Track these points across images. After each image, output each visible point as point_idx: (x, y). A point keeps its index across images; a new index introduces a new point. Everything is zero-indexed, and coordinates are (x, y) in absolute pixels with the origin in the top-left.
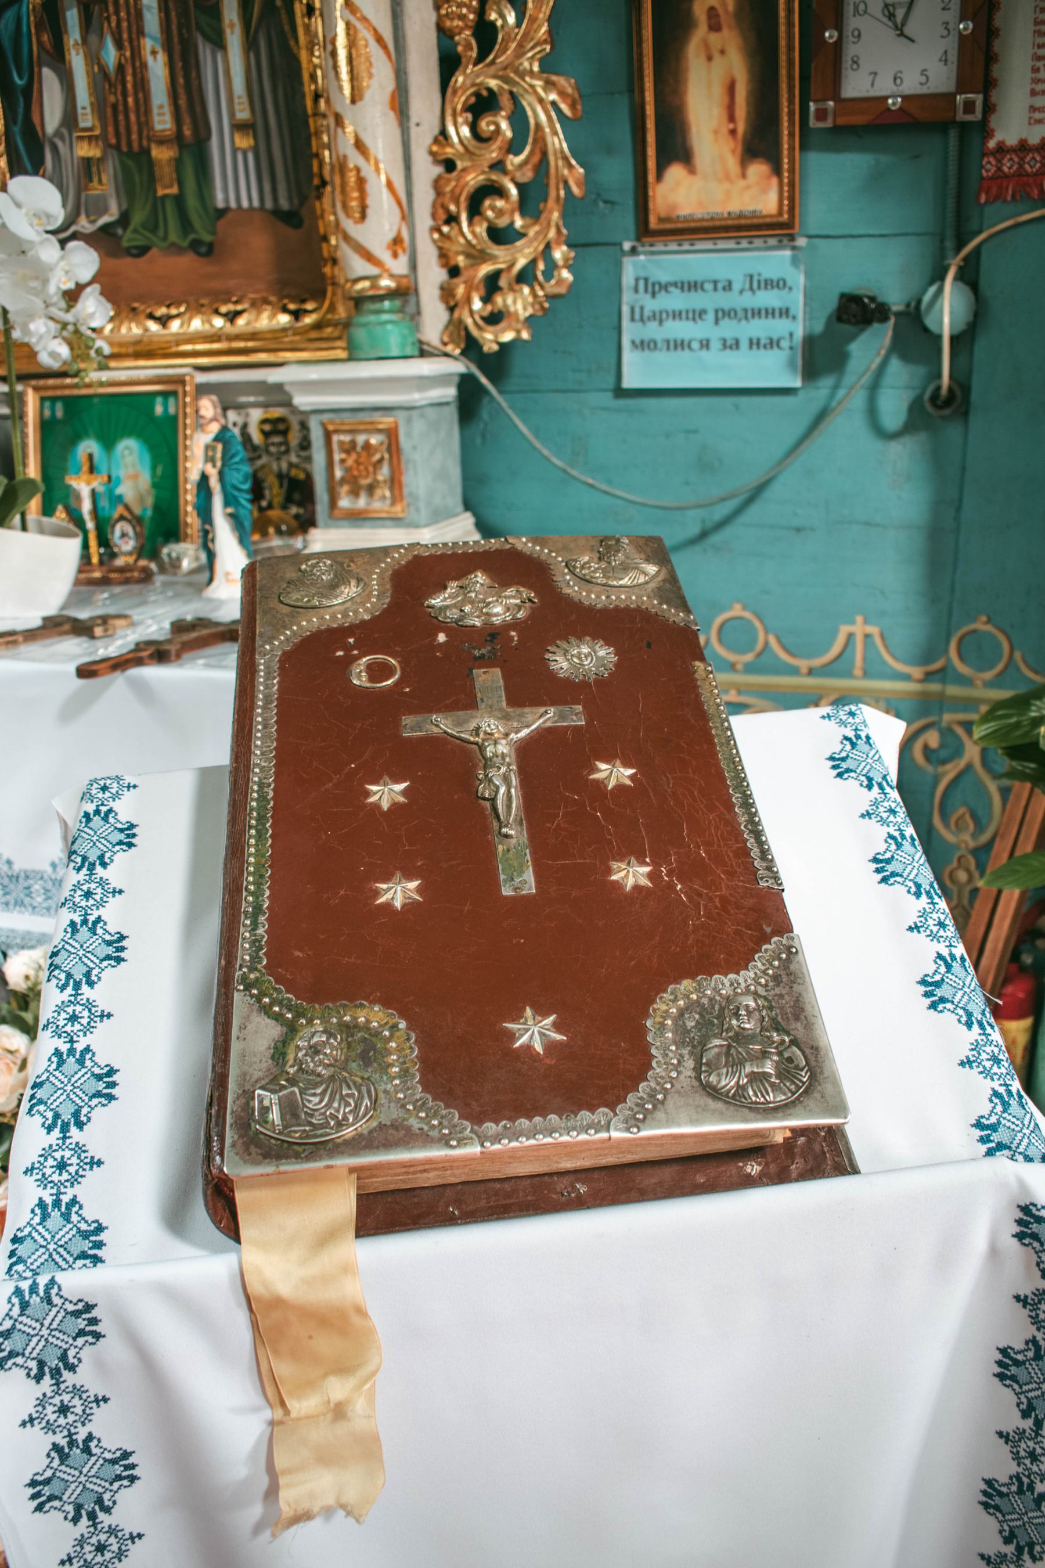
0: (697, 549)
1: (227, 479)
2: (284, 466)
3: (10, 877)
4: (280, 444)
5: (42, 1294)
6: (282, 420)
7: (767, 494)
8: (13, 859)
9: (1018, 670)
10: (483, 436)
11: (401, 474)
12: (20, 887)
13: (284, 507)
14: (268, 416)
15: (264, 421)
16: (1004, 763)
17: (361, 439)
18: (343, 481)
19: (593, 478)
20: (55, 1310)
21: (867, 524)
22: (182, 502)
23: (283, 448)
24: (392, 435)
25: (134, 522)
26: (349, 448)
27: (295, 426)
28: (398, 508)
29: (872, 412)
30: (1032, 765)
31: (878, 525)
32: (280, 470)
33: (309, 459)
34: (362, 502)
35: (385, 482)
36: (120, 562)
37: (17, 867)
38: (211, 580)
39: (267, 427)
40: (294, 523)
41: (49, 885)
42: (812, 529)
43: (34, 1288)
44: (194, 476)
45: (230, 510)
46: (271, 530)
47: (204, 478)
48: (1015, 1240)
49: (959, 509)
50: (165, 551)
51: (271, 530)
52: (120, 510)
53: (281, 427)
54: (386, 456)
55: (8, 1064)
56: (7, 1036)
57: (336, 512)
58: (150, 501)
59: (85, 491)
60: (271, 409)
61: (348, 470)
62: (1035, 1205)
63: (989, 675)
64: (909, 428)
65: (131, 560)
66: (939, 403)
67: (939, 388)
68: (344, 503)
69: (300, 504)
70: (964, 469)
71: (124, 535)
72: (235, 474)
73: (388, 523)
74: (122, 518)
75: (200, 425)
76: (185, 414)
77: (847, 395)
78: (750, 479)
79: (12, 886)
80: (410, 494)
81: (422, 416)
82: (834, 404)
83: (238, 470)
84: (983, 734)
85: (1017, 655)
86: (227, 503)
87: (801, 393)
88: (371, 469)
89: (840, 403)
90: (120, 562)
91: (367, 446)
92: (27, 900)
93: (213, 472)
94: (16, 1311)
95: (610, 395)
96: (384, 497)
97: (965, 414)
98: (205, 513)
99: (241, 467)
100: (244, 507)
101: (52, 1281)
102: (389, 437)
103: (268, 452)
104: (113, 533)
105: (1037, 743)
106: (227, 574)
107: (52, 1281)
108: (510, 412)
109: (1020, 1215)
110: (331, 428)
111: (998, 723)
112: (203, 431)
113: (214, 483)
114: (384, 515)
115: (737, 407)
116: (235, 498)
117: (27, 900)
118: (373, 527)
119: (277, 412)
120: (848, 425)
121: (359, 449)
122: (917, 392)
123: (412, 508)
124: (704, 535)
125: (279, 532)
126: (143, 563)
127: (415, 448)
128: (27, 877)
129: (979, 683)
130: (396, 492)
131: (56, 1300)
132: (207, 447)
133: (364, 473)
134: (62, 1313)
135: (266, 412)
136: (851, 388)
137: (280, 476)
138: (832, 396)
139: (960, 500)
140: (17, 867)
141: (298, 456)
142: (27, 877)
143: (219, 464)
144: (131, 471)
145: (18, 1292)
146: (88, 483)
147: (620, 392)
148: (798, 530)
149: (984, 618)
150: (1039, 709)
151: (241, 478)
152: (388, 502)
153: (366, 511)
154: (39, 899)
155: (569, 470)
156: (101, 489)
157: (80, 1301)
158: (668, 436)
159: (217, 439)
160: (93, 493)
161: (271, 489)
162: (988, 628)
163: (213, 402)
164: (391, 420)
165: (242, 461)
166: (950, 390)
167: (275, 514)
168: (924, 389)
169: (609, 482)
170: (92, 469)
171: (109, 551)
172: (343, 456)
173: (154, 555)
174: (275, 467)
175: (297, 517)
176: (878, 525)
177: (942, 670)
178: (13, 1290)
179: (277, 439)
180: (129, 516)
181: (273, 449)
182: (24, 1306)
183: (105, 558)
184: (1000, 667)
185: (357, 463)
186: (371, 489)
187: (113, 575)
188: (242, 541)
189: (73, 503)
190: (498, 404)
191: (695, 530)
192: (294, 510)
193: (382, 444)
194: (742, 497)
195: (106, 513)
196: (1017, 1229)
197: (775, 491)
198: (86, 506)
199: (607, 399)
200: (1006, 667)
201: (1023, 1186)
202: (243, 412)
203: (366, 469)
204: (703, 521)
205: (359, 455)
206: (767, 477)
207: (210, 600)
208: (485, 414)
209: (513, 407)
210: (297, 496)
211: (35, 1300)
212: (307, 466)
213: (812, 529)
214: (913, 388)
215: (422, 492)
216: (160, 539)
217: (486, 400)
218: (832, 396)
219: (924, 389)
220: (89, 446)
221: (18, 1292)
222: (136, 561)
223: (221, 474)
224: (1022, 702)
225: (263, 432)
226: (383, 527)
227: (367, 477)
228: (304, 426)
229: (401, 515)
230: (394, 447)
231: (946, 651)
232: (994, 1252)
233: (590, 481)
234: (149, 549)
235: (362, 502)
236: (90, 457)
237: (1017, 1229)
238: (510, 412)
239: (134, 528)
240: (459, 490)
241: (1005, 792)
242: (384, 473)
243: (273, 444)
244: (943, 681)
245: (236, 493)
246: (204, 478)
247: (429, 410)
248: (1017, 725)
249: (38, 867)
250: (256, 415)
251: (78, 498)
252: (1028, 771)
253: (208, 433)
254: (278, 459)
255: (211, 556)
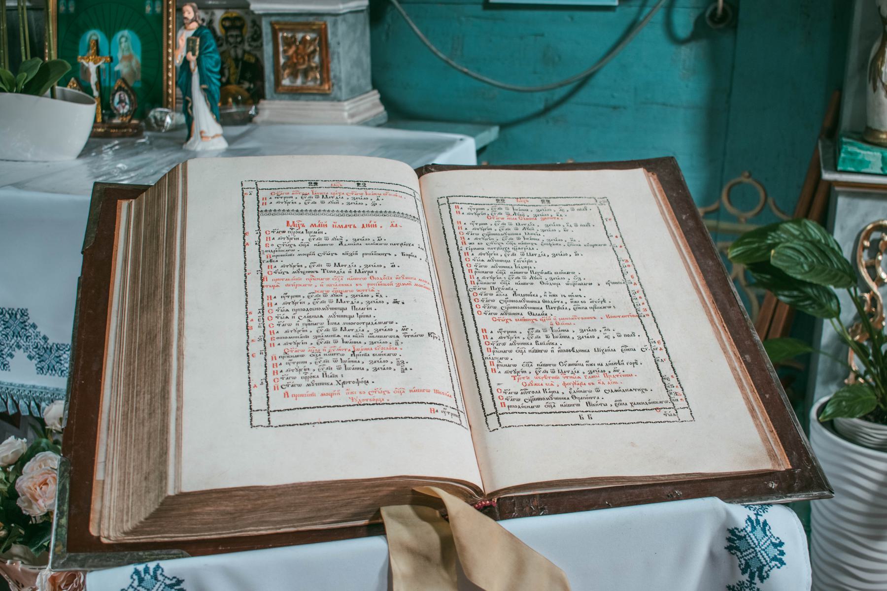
0: (542, 120)
2: (240, 52)
3: (45, 349)
4: (237, 36)
5: (152, 573)
6: (238, 18)
7: (593, 81)
8: (48, 336)
11: (328, 62)
12: (53, 356)
13: (239, 83)
14: (229, 15)
15: (224, 19)
17: (299, 36)
18: (285, 65)
20: (159, 583)
21: (664, 104)
23: (239, 39)
24: (322, 35)
26: (289, 43)
27: (249, 24)
30: (768, 277)
31: (671, 106)
32: (237, 56)
33: (260, 47)
35: (317, 68)
36: (117, 121)
39: (227, 24)
40: (246, 94)
42: (625, 108)
43: (146, 570)
44: (178, 61)
45: (204, 86)
47: (186, 62)
48: (725, 552)
52: (119, 82)
53: (238, 24)
54: (318, 49)
58: (139, 77)
59: (93, 68)
61: (289, 58)
62: (737, 529)
63: (750, 214)
65: (126, 120)
67: (716, 9)
68: (286, 82)
72: (209, 60)
73: (318, 97)
74: (120, 89)
75: (182, 23)
78: (580, 71)
79: (46, 356)
80: (335, 77)
81: (344, 20)
82: (641, 18)
83: (211, 58)
84: (734, 254)
85: (770, 201)
86: (202, 82)
87: (618, 10)
88: (306, 58)
89: (646, 17)
91: (304, 40)
93: (192, 58)
94: (136, 583)
95: (480, 7)
97: (735, 27)
99: (213, 55)
100: (214, 84)
101: (158, 567)
102: (320, 35)
103: (227, 42)
104: (113, 100)
105: (769, 261)
107: (158, 567)
108: (408, 18)
111: (745, 247)
112: (185, 28)
113: (193, 65)
114: (315, 92)
119: (235, 13)
123: (335, 87)
124: (547, 110)
125: (236, 102)
126: (134, 122)
131: (160, 578)
132: (188, 40)
133: (301, 61)
136: (654, 7)
137: (236, 60)
140: (50, 342)
141: (250, 45)
143: (197, 53)
144: (126, 54)
147: (488, 6)
148: (615, 108)
149: (747, 174)
150: (774, 238)
151: (214, 64)
157: (174, 578)
158: (522, 38)
159: (195, 35)
160: (98, 68)
162: (750, 180)
163: (192, 7)
166: (724, 9)
167: (233, 88)
168: (706, 9)
169: (479, 70)
170: (98, 52)
171: (108, 112)
173: (143, 116)
174: (232, 52)
175: (248, 90)
177: (717, 210)
178: (133, 570)
181: (231, 40)
182: (141, 580)
183: (106, 118)
185: (296, 52)
186: (306, 73)
188: (212, 110)
191: (541, 106)
192: (246, 85)
193: (315, 40)
194: (575, 84)
197: (600, 79)
198: (93, 79)
199: (478, 9)
201: (728, 514)
202: (210, 12)
203: (303, 57)
204: (546, 100)
206: (592, 71)
208: (388, 19)
210: (248, 75)
211: (148, 577)
212: (258, 54)
214: (698, 8)
215: (343, 76)
219: (706, 9)
222: (130, 120)
223: (199, 61)
225: (223, 26)
226: (314, 100)
227: (304, 63)
231: (720, 197)
232: (712, 557)
233: (465, 70)
234: (139, 112)
236: (97, 41)
239: (129, 97)
240: (369, 73)
243: (232, 36)
244: (718, 219)
245: (209, 74)
246: (186, 62)
247: (349, 16)
248: (758, 249)
250: (219, 14)
252: (764, 280)
254: (235, 47)
255: (190, 120)
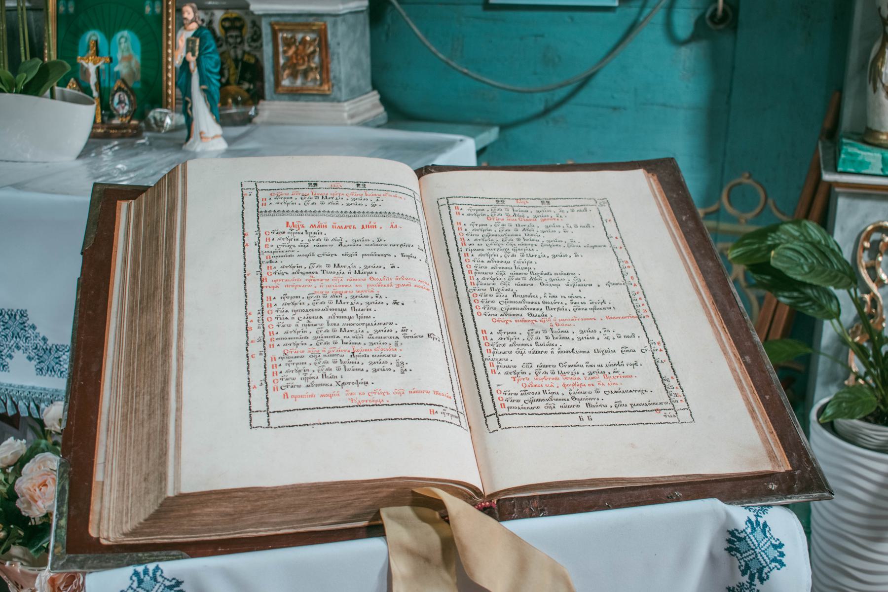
2: (239, 52)
3: (45, 350)
4: (237, 37)
5: (151, 575)
6: (238, 19)
7: (593, 82)
8: (47, 337)
9: (771, 212)
10: (387, 35)
11: (328, 63)
12: (52, 357)
13: (239, 84)
14: (229, 16)
15: (224, 20)
17: (299, 36)
18: (285, 67)
19: (467, 68)
20: (158, 585)
22: (165, 78)
23: (239, 40)
24: (322, 35)
26: (288, 43)
27: (248, 24)
30: (768, 278)
31: (672, 107)
32: (236, 56)
35: (316, 68)
36: (116, 121)
39: (227, 24)
40: (246, 95)
42: (625, 109)
43: (146, 572)
44: (178, 62)
45: (204, 87)
47: (186, 63)
49: (729, 96)
52: (119, 83)
53: (238, 24)
57: (280, 89)
58: (139, 77)
59: (92, 69)
60: (230, 11)
61: (289, 59)
62: (737, 530)
63: (750, 215)
64: (694, 37)
65: (126, 120)
66: (716, 20)
67: (716, 10)
68: (286, 82)
69: (250, 82)
70: (733, 68)
71: (121, 102)
72: (209, 61)
73: (318, 98)
74: (120, 89)
77: (651, 13)
78: (581, 72)
79: (45, 357)
80: (335, 77)
81: (344, 20)
82: (641, 19)
83: (211, 58)
84: (734, 255)
86: (202, 83)
88: (306, 59)
89: (646, 19)
90: (116, 121)
91: (303, 42)
92: (57, 367)
93: (192, 59)
94: (135, 585)
95: (480, 8)
96: (315, 79)
98: (186, 90)
99: (213, 55)
100: (214, 84)
101: (157, 568)
103: (227, 42)
104: (113, 100)
105: (769, 262)
107: (157, 568)
108: (408, 19)
109: (730, 537)
112: (185, 29)
113: (193, 66)
114: (315, 92)
115: (572, 19)
117: (57, 367)
118: (307, 101)
119: (235, 13)
120: (651, 33)
122: (701, 11)
124: (546, 112)
125: (236, 103)
126: (134, 122)
129: (743, 221)
130: (324, 76)
131: (160, 579)
132: (188, 41)
133: (301, 62)
134: (163, 587)
136: (654, 8)
137: (236, 60)
138: (640, 13)
139: (731, 89)
140: (50, 343)
141: (250, 46)
143: (197, 53)
144: (126, 54)
145: (136, 573)
147: (488, 6)
148: (615, 109)
149: (747, 175)
150: (773, 239)
151: (213, 64)
153: (302, 89)
155: (450, 62)
156: (103, 67)
159: (194, 35)
161: (229, 69)
162: (750, 181)
163: (192, 7)
166: (724, 10)
167: (232, 88)
168: (706, 10)
170: (97, 53)
171: (108, 113)
172: (285, 48)
173: (143, 117)
174: (232, 53)
176: (672, 107)
177: (717, 211)
178: (133, 572)
179: (234, 33)
180: (126, 89)
181: (231, 40)
182: (140, 582)
183: (106, 118)
186: (305, 74)
189: (80, 77)
190: (400, 13)
191: (541, 107)
192: (246, 86)
193: (315, 40)
195: (107, 84)
196: (727, 545)
197: (600, 79)
198: (93, 80)
199: (478, 10)
200: (762, 210)
202: (209, 12)
204: (546, 101)
206: (593, 71)
208: (389, 19)
209: (408, 15)
211: (147, 578)
212: (258, 54)
213: (625, 109)
214: (698, 9)
216: (147, 105)
217: (389, 8)
218: (640, 13)
219: (706, 10)
220: (93, 35)
221: (136, 573)
222: (129, 121)
223: (198, 62)
225: (223, 27)
226: (314, 101)
227: (303, 64)
228: (256, 24)
229: (328, 93)
230: (323, 43)
232: (712, 558)
233: (466, 71)
234: (139, 113)
235: (299, 82)
236: (96, 42)
237: (727, 545)
238: (408, 19)
239: (129, 98)
240: (369, 74)
241: (761, 299)
243: (231, 36)
244: (718, 219)
245: (209, 75)
246: (186, 63)
248: (758, 250)
251: (86, 72)
253: (190, 30)
254: (235, 47)
255: (189, 120)
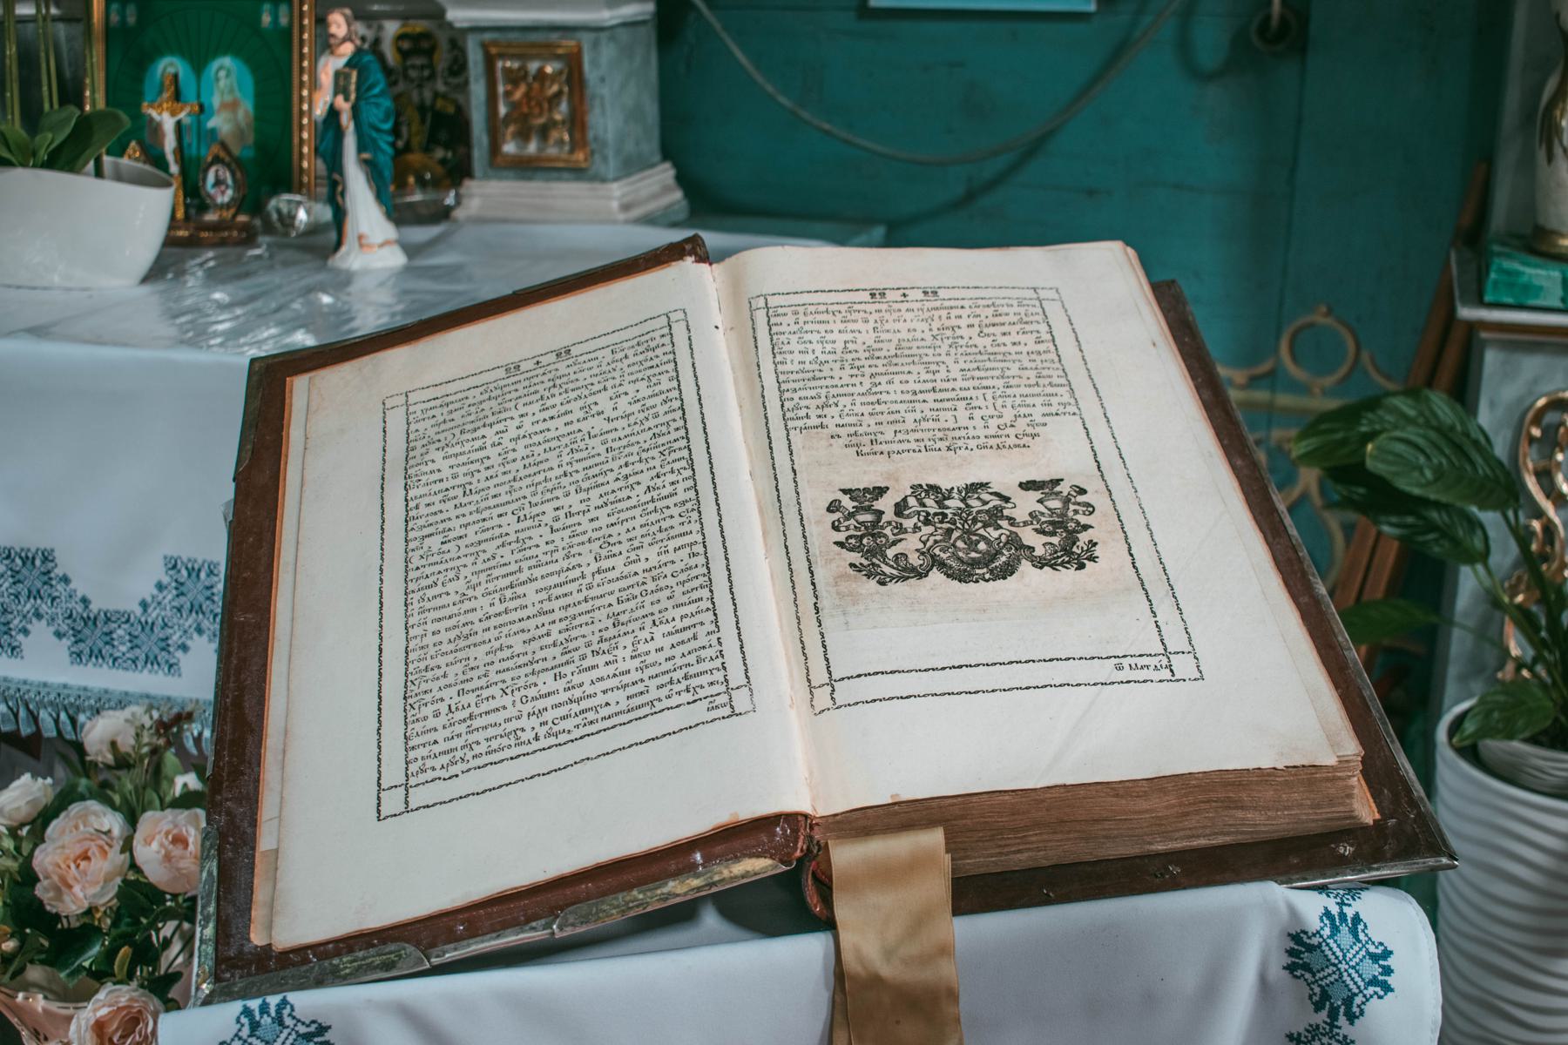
1: (364, 116)
2: (428, 95)
3: (86, 621)
4: (422, 67)
5: (273, 1014)
6: (426, 36)
8: (89, 596)
12: (98, 632)
13: (427, 150)
14: (409, 30)
16: (1337, 492)
17: (533, 66)
18: (508, 120)
20: (286, 1032)
23: (426, 73)
25: (233, 166)
26: (514, 78)
28: (580, 156)
29: (1184, 46)
30: (1361, 490)
34: (532, 147)
35: (563, 122)
36: (211, 217)
37: (94, 608)
38: (339, 244)
39: (406, 45)
40: (440, 170)
41: (137, 630)
43: (264, 1009)
44: (320, 111)
45: (366, 156)
46: (411, 180)
50: (273, 203)
51: (411, 180)
52: (215, 149)
53: (425, 45)
54: (566, 89)
55: (101, 847)
56: (96, 814)
57: (499, 159)
58: (250, 139)
59: (168, 123)
61: (514, 106)
63: (1329, 381)
65: (228, 214)
67: (1268, 18)
68: (509, 148)
69: (447, 146)
71: (218, 182)
72: (375, 110)
73: (566, 175)
74: (217, 160)
75: (326, 44)
76: (302, 27)
81: (612, 38)
83: (377, 105)
84: (1302, 451)
86: (361, 148)
88: (546, 105)
91: (541, 75)
92: (106, 650)
93: (343, 105)
96: (561, 142)
97: (1303, 50)
100: (382, 151)
101: (284, 1002)
103: (406, 77)
106: (360, 237)
107: (284, 1002)
108: (724, 35)
110: (494, 51)
112: (332, 53)
113: (346, 119)
114: (561, 165)
116: (374, 141)
117: (106, 650)
118: (548, 180)
119: (419, 26)
121: (530, 79)
124: (970, 196)
125: (422, 183)
127: (603, 80)
128: (108, 620)
129: (1317, 390)
130: (577, 136)
131: (288, 1021)
132: (337, 74)
133: (536, 111)
135: (403, 26)
137: (422, 109)
141: (446, 84)
142: (108, 620)
143: (353, 97)
144: (228, 98)
145: (247, 1012)
146: (173, 114)
148: (1091, 193)
149: (1324, 309)
151: (381, 115)
152: (567, 148)
154: (123, 649)
157: (314, 1022)
159: (349, 64)
160: (179, 124)
162: (1329, 321)
163: (345, 15)
164: (572, 43)
165: (382, 94)
166: (1283, 18)
167: (415, 158)
170: (177, 96)
172: (509, 87)
175: (443, 162)
177: (1272, 374)
178: (240, 1009)
179: (419, 61)
180: (227, 159)
181: (413, 74)
182: (255, 1026)
183: (193, 211)
184: (1343, 370)
185: (527, 95)
186: (544, 132)
187: (205, 235)
192: (439, 153)
193: (560, 72)
195: (194, 151)
198: (170, 143)
201: (1293, 912)
202: (375, 24)
205: (530, 86)
207: (337, 272)
210: (443, 135)
211: (266, 1020)
212: (460, 98)
215: (610, 136)
220: (170, 65)
222: (234, 216)
223: (356, 112)
224: (1350, 415)
225: (399, 50)
226: (559, 179)
227: (541, 114)
229: (583, 165)
231: (1276, 350)
233: (827, 126)
234: (252, 201)
236: (176, 76)
238: (724, 35)
240: (656, 133)
241: (1348, 529)
242: (562, 111)
243: (413, 67)
244: (1273, 389)
245: (374, 134)
246: (333, 113)
248: (1343, 442)
249: (122, 606)
250: (392, 28)
254: (420, 86)
255: (340, 215)
